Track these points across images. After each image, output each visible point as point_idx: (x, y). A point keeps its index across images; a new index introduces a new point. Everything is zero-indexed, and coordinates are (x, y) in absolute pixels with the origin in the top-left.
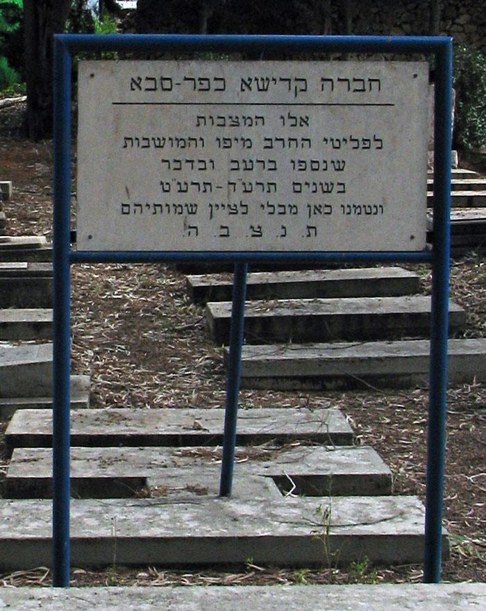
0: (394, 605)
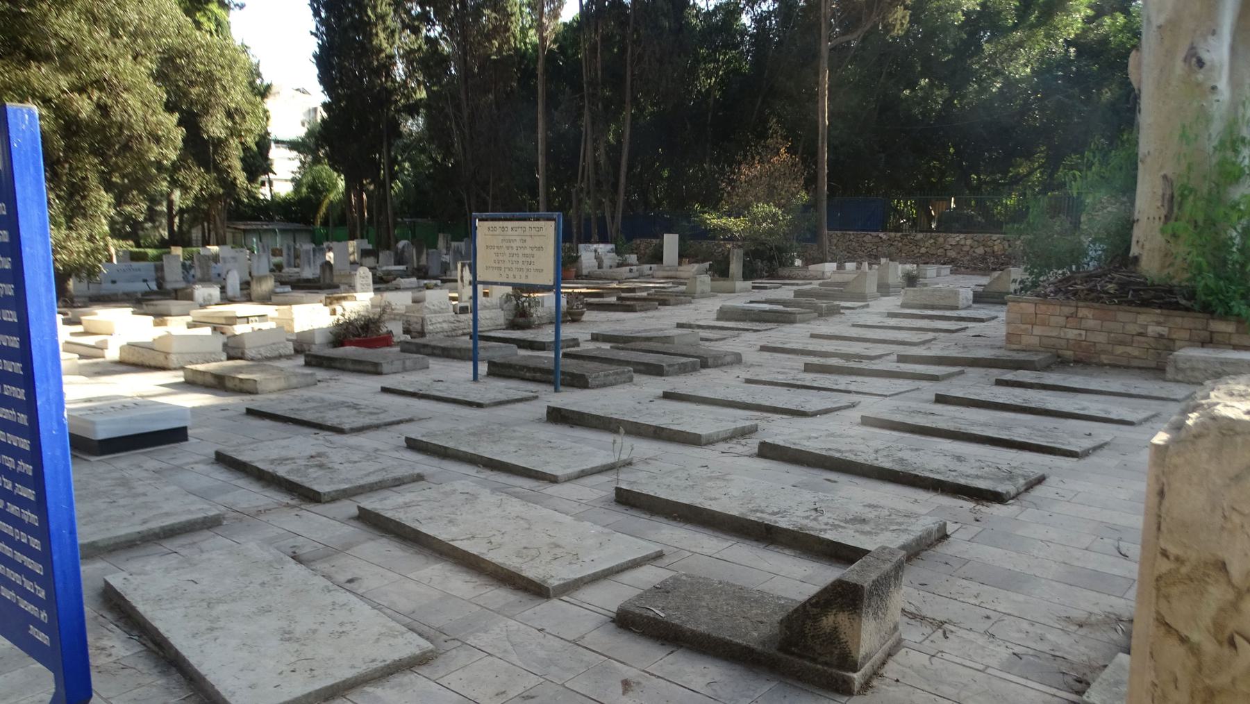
0: (874, 576)
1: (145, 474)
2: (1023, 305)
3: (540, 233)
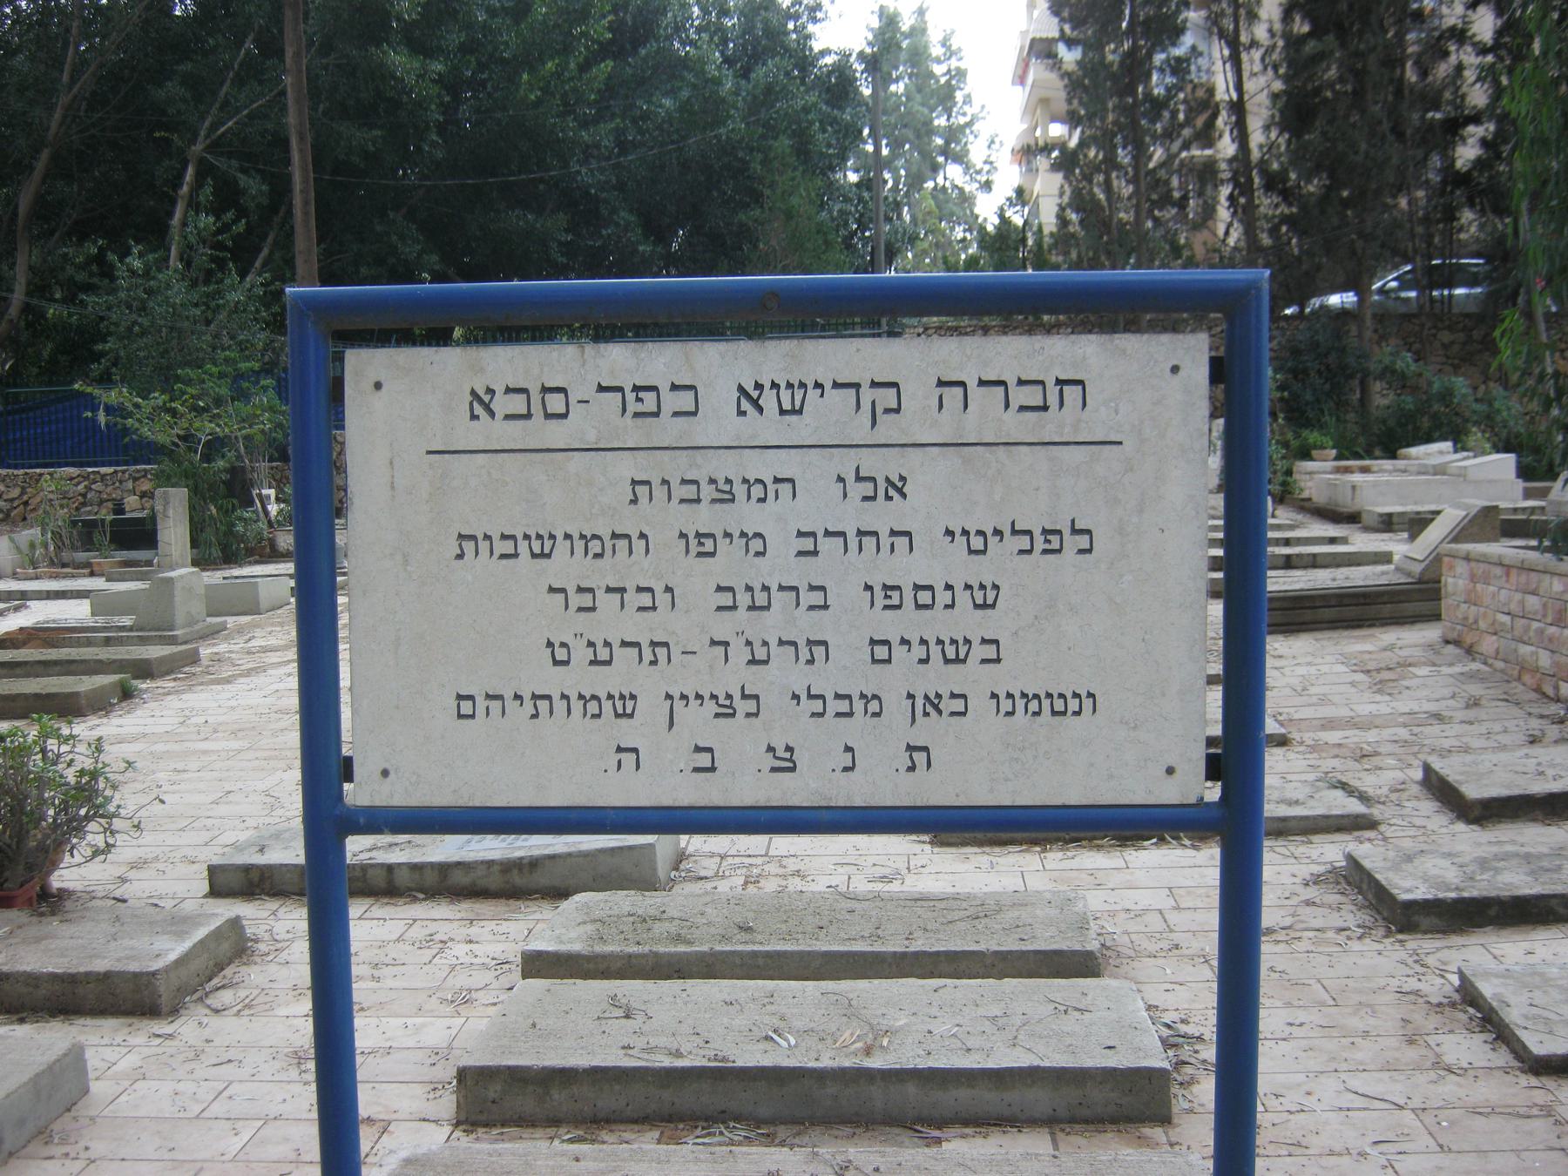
1: (1308, 737)
3: (1051, 425)
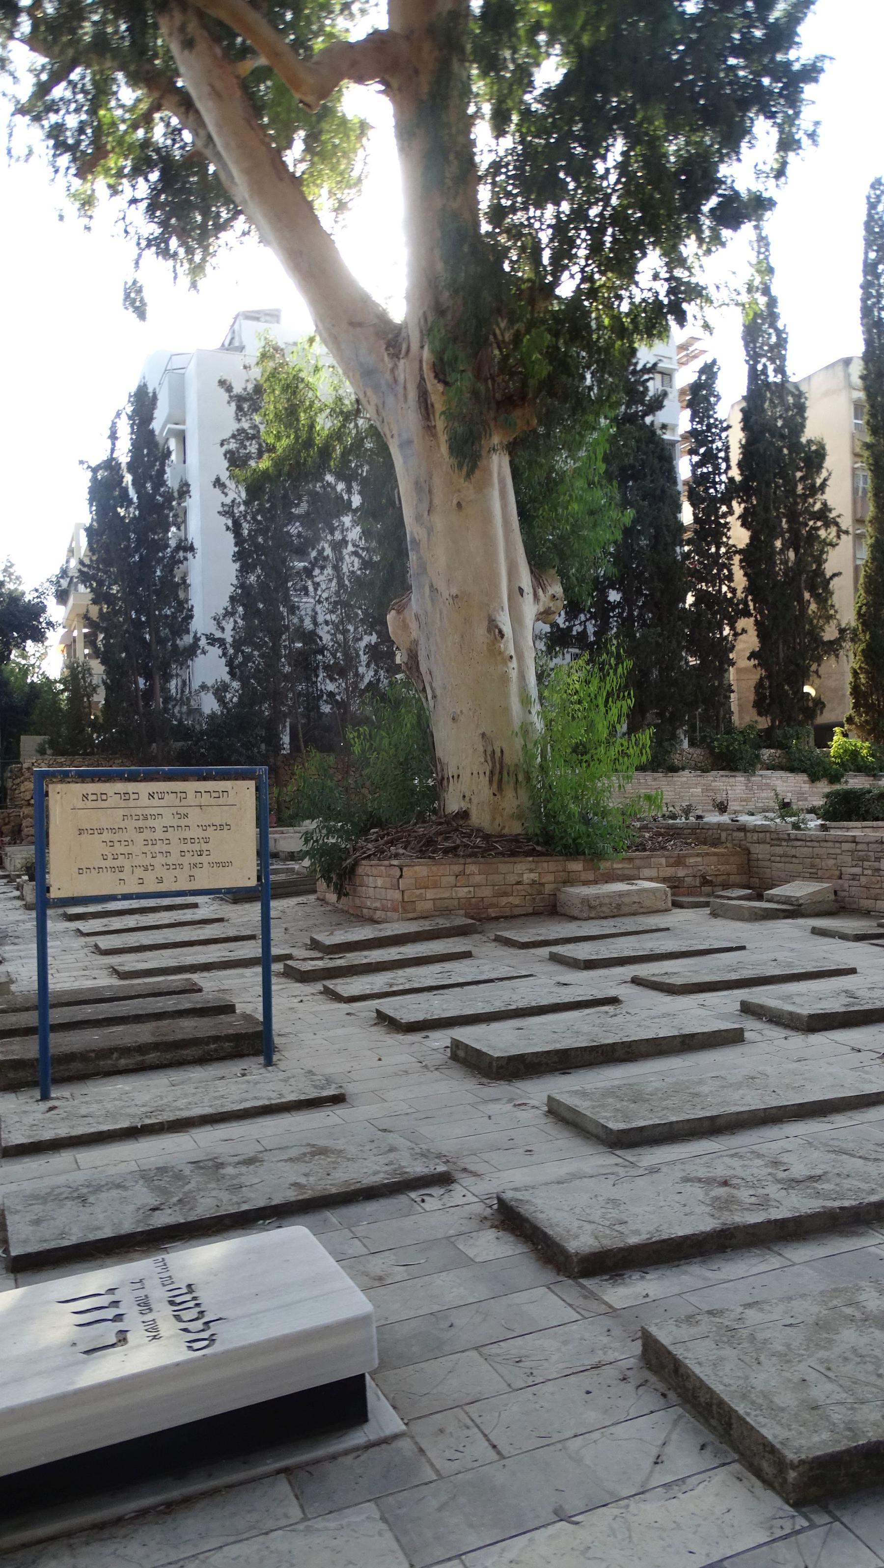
2: (416, 868)
3: (221, 801)
